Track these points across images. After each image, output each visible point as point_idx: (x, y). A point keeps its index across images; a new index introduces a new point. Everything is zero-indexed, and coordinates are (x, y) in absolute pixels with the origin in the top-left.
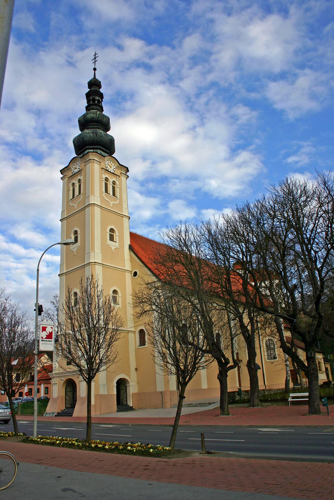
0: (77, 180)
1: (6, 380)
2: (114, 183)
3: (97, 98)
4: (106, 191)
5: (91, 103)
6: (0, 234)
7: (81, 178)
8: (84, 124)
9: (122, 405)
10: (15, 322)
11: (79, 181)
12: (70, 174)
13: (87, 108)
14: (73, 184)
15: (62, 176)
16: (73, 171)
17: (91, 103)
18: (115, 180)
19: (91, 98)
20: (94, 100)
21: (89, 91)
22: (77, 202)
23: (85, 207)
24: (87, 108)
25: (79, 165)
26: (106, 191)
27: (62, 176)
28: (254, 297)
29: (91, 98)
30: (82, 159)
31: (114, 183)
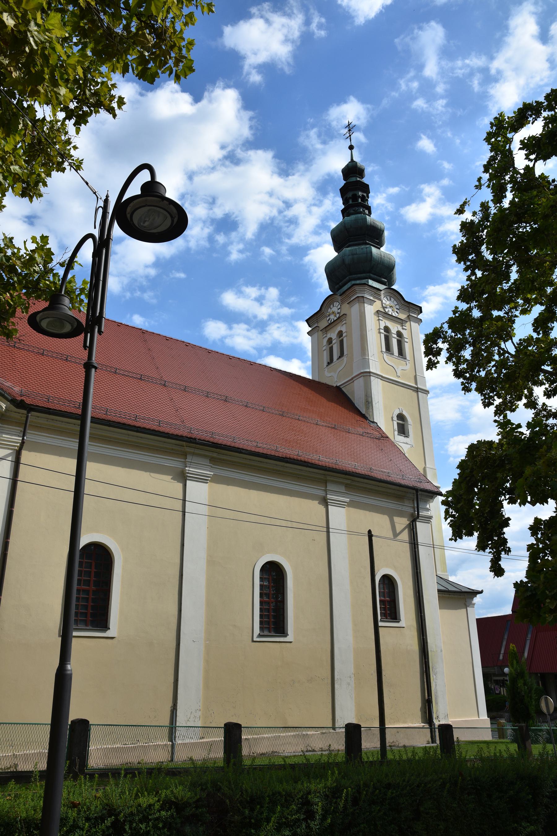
0: (337, 332)
1: (102, 46)
2: (399, 334)
3: (360, 194)
4: (388, 348)
5: (351, 202)
6: (136, 1)
7: (344, 329)
8: (340, 238)
9: (536, 674)
10: (166, 795)
11: (340, 334)
12: (323, 324)
13: (343, 211)
14: (330, 341)
15: (310, 329)
16: (328, 319)
17: (351, 202)
18: (400, 329)
19: (350, 195)
20: (355, 197)
21: (345, 184)
22: (338, 371)
23: (352, 379)
24: (344, 212)
25: (339, 306)
26: (388, 348)
27: (310, 329)
28: (269, 583)
29: (350, 195)
30: (344, 296)
31: (399, 334)
